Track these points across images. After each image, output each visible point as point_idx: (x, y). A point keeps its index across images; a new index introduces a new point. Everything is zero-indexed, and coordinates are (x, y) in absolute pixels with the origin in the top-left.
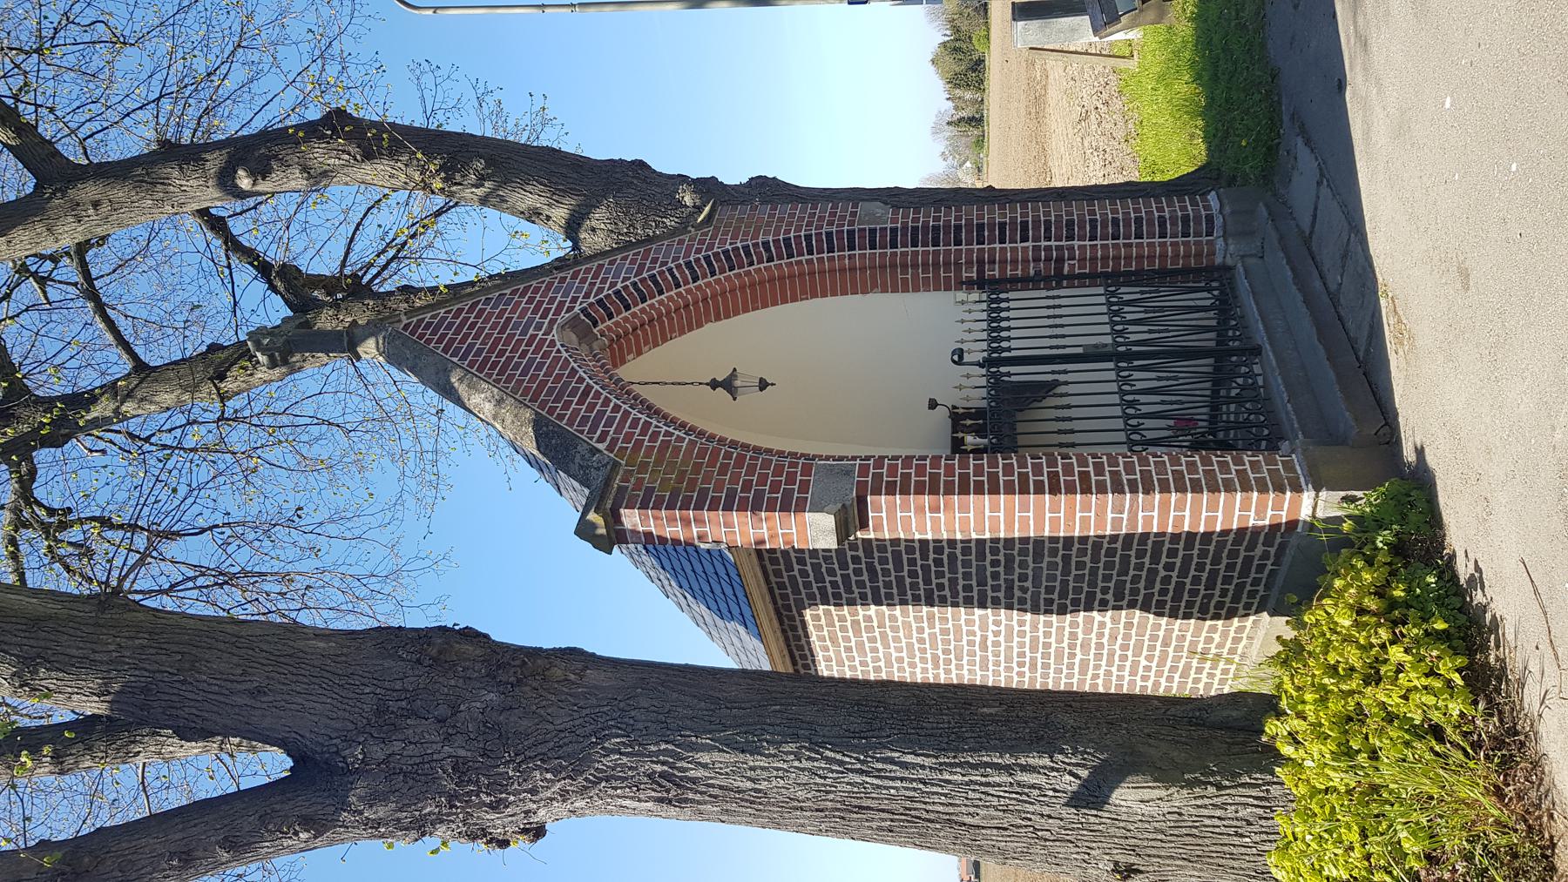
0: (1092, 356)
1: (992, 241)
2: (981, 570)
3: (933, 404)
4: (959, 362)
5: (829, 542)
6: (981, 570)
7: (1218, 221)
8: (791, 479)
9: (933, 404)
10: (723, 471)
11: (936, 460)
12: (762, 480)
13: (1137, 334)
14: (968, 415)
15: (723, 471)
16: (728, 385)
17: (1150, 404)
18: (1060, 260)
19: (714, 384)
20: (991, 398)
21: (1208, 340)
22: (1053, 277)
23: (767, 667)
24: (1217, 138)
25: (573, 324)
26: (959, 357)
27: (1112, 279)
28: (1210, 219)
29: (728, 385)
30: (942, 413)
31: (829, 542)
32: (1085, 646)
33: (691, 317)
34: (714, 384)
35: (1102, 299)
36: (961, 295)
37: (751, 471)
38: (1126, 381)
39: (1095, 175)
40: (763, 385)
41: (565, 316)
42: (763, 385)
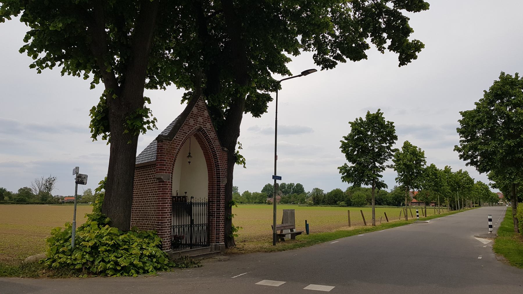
2: (152, 201)
3: (186, 193)
5: (392, 8)
6: (152, 201)
8: (168, 170)
9: (186, 193)
10: (170, 159)
11: (171, 194)
13: (196, 229)
14: (185, 199)
15: (170, 159)
16: (189, 156)
18: (212, 216)
19: (190, 153)
20: (188, 203)
23: (136, 163)
25: (201, 128)
27: (209, 226)
29: (189, 156)
30: (184, 195)
31: (392, 8)
32: (139, 220)
34: (190, 153)
35: (178, 224)
36: (207, 198)
41: (202, 126)
42: (189, 162)
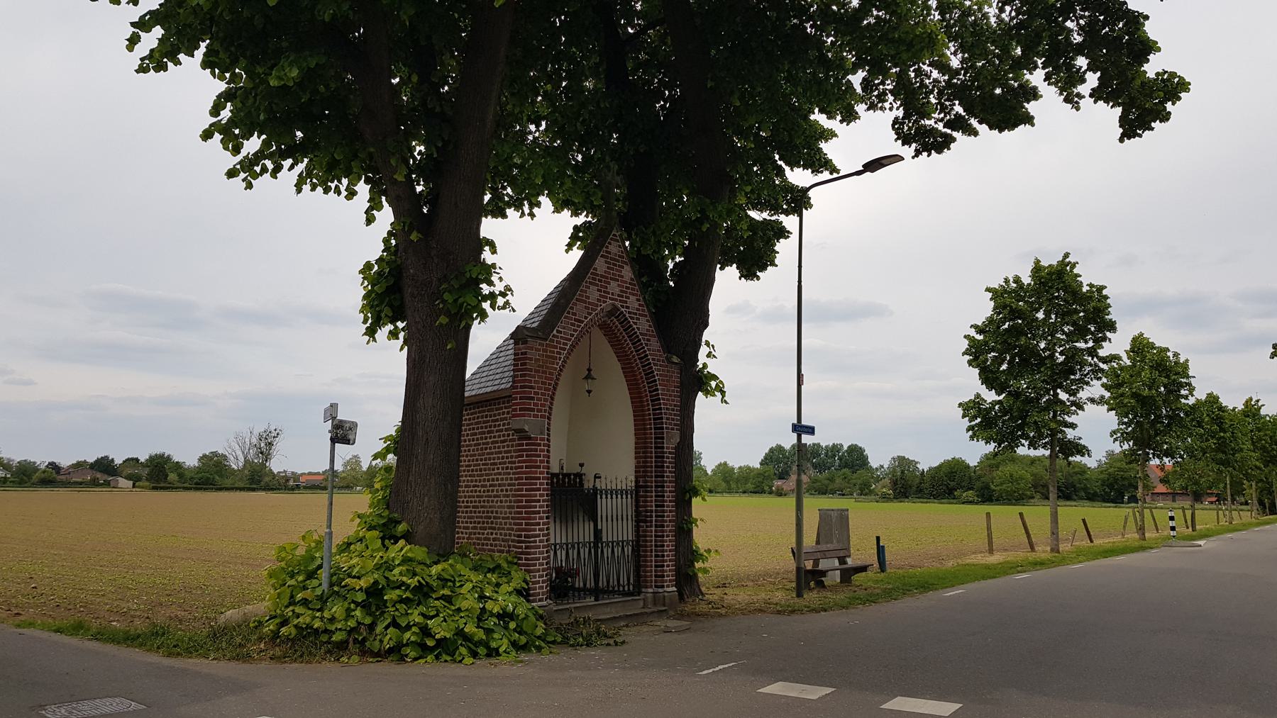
0: (598, 533)
3: (582, 465)
4: (596, 477)
8: (539, 411)
9: (582, 465)
12: (539, 399)
13: (607, 552)
14: (581, 480)
17: (573, 554)
18: (646, 521)
19: (589, 370)
21: (602, 583)
22: (640, 518)
23: (467, 394)
24: (198, 470)
25: (615, 308)
26: (597, 477)
27: (638, 545)
30: (578, 469)
32: (475, 528)
33: (622, 356)
34: (589, 370)
37: (543, 394)
38: (584, 545)
39: (701, 538)
40: (589, 392)
41: (618, 304)
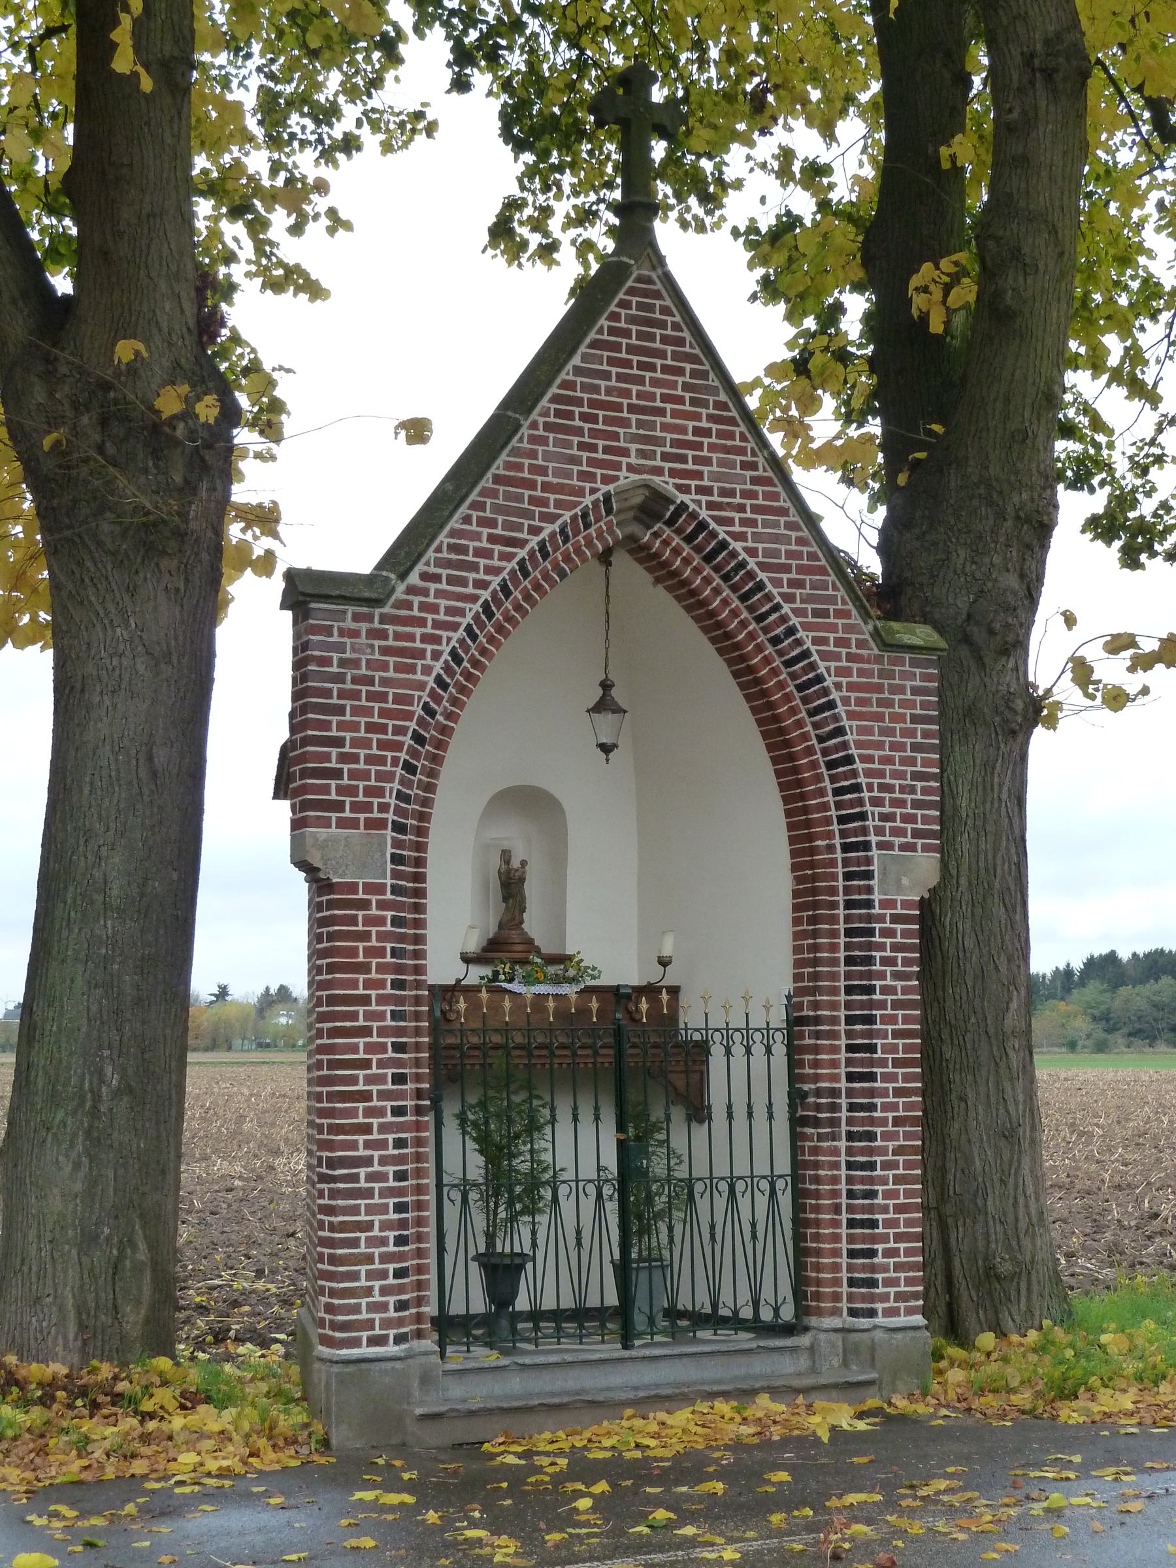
1: (849, 1035)
7: (864, 1322)
16: (605, 705)
28: (872, 1313)
34: (606, 686)
40: (606, 749)
